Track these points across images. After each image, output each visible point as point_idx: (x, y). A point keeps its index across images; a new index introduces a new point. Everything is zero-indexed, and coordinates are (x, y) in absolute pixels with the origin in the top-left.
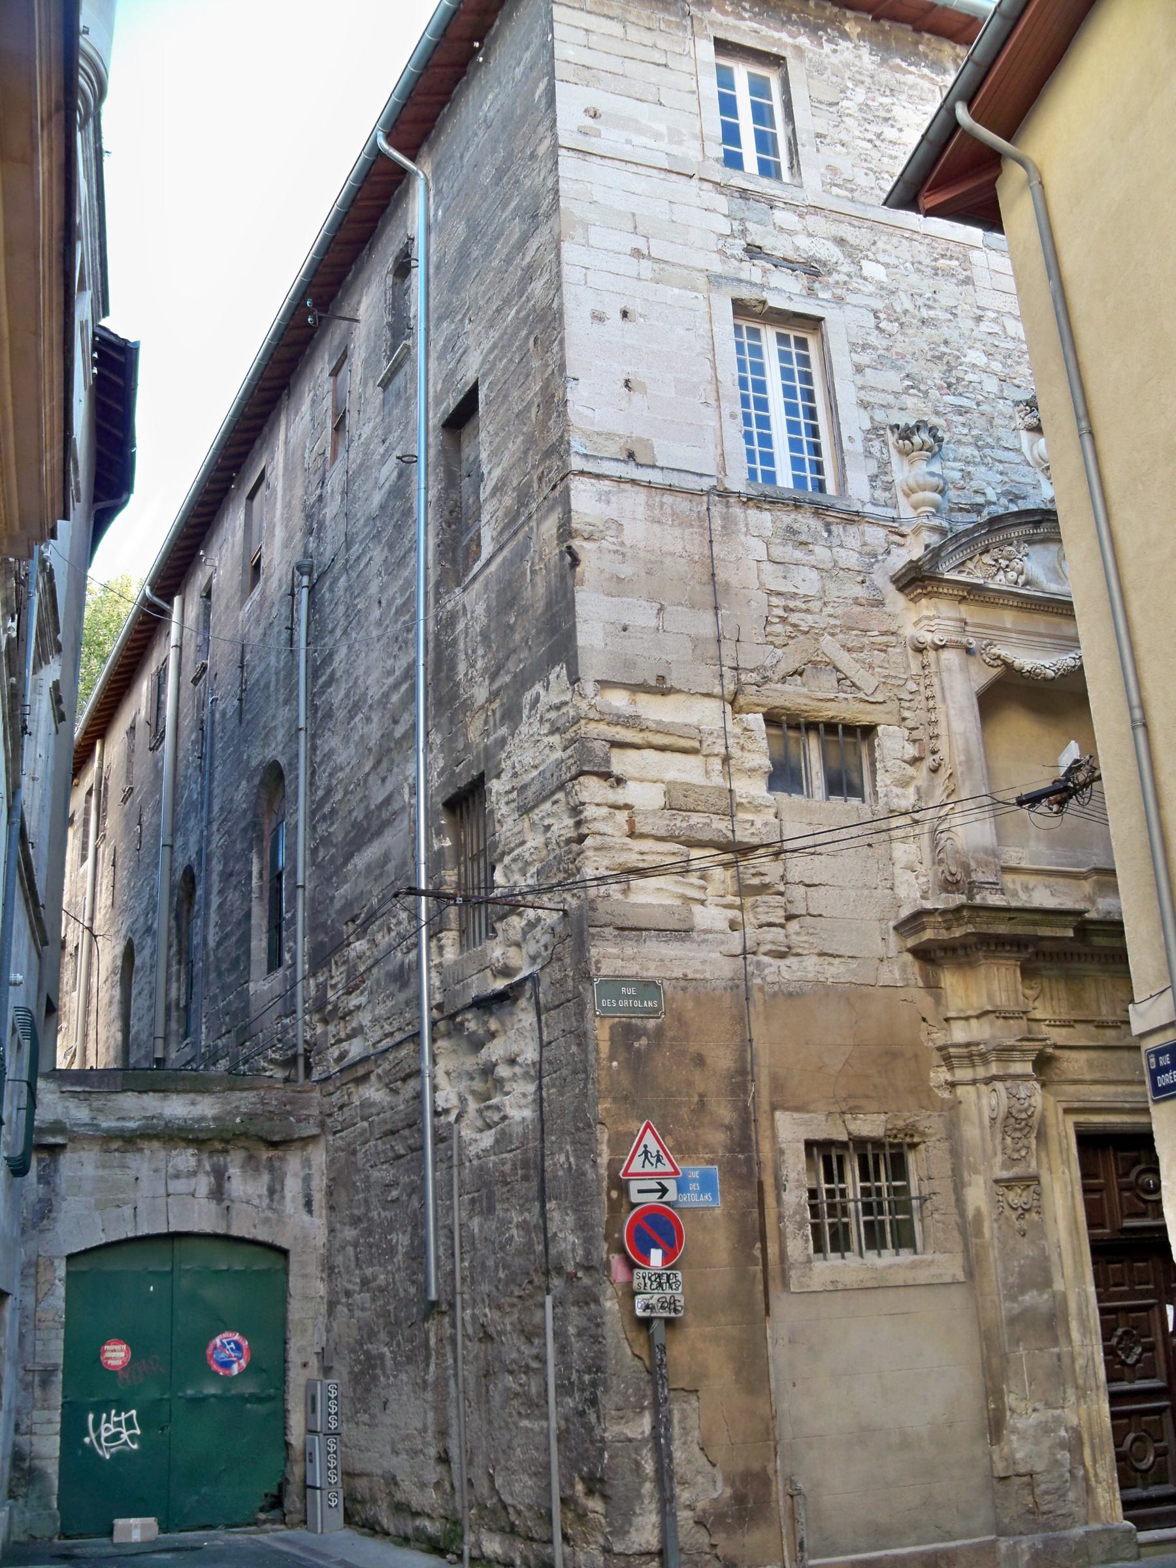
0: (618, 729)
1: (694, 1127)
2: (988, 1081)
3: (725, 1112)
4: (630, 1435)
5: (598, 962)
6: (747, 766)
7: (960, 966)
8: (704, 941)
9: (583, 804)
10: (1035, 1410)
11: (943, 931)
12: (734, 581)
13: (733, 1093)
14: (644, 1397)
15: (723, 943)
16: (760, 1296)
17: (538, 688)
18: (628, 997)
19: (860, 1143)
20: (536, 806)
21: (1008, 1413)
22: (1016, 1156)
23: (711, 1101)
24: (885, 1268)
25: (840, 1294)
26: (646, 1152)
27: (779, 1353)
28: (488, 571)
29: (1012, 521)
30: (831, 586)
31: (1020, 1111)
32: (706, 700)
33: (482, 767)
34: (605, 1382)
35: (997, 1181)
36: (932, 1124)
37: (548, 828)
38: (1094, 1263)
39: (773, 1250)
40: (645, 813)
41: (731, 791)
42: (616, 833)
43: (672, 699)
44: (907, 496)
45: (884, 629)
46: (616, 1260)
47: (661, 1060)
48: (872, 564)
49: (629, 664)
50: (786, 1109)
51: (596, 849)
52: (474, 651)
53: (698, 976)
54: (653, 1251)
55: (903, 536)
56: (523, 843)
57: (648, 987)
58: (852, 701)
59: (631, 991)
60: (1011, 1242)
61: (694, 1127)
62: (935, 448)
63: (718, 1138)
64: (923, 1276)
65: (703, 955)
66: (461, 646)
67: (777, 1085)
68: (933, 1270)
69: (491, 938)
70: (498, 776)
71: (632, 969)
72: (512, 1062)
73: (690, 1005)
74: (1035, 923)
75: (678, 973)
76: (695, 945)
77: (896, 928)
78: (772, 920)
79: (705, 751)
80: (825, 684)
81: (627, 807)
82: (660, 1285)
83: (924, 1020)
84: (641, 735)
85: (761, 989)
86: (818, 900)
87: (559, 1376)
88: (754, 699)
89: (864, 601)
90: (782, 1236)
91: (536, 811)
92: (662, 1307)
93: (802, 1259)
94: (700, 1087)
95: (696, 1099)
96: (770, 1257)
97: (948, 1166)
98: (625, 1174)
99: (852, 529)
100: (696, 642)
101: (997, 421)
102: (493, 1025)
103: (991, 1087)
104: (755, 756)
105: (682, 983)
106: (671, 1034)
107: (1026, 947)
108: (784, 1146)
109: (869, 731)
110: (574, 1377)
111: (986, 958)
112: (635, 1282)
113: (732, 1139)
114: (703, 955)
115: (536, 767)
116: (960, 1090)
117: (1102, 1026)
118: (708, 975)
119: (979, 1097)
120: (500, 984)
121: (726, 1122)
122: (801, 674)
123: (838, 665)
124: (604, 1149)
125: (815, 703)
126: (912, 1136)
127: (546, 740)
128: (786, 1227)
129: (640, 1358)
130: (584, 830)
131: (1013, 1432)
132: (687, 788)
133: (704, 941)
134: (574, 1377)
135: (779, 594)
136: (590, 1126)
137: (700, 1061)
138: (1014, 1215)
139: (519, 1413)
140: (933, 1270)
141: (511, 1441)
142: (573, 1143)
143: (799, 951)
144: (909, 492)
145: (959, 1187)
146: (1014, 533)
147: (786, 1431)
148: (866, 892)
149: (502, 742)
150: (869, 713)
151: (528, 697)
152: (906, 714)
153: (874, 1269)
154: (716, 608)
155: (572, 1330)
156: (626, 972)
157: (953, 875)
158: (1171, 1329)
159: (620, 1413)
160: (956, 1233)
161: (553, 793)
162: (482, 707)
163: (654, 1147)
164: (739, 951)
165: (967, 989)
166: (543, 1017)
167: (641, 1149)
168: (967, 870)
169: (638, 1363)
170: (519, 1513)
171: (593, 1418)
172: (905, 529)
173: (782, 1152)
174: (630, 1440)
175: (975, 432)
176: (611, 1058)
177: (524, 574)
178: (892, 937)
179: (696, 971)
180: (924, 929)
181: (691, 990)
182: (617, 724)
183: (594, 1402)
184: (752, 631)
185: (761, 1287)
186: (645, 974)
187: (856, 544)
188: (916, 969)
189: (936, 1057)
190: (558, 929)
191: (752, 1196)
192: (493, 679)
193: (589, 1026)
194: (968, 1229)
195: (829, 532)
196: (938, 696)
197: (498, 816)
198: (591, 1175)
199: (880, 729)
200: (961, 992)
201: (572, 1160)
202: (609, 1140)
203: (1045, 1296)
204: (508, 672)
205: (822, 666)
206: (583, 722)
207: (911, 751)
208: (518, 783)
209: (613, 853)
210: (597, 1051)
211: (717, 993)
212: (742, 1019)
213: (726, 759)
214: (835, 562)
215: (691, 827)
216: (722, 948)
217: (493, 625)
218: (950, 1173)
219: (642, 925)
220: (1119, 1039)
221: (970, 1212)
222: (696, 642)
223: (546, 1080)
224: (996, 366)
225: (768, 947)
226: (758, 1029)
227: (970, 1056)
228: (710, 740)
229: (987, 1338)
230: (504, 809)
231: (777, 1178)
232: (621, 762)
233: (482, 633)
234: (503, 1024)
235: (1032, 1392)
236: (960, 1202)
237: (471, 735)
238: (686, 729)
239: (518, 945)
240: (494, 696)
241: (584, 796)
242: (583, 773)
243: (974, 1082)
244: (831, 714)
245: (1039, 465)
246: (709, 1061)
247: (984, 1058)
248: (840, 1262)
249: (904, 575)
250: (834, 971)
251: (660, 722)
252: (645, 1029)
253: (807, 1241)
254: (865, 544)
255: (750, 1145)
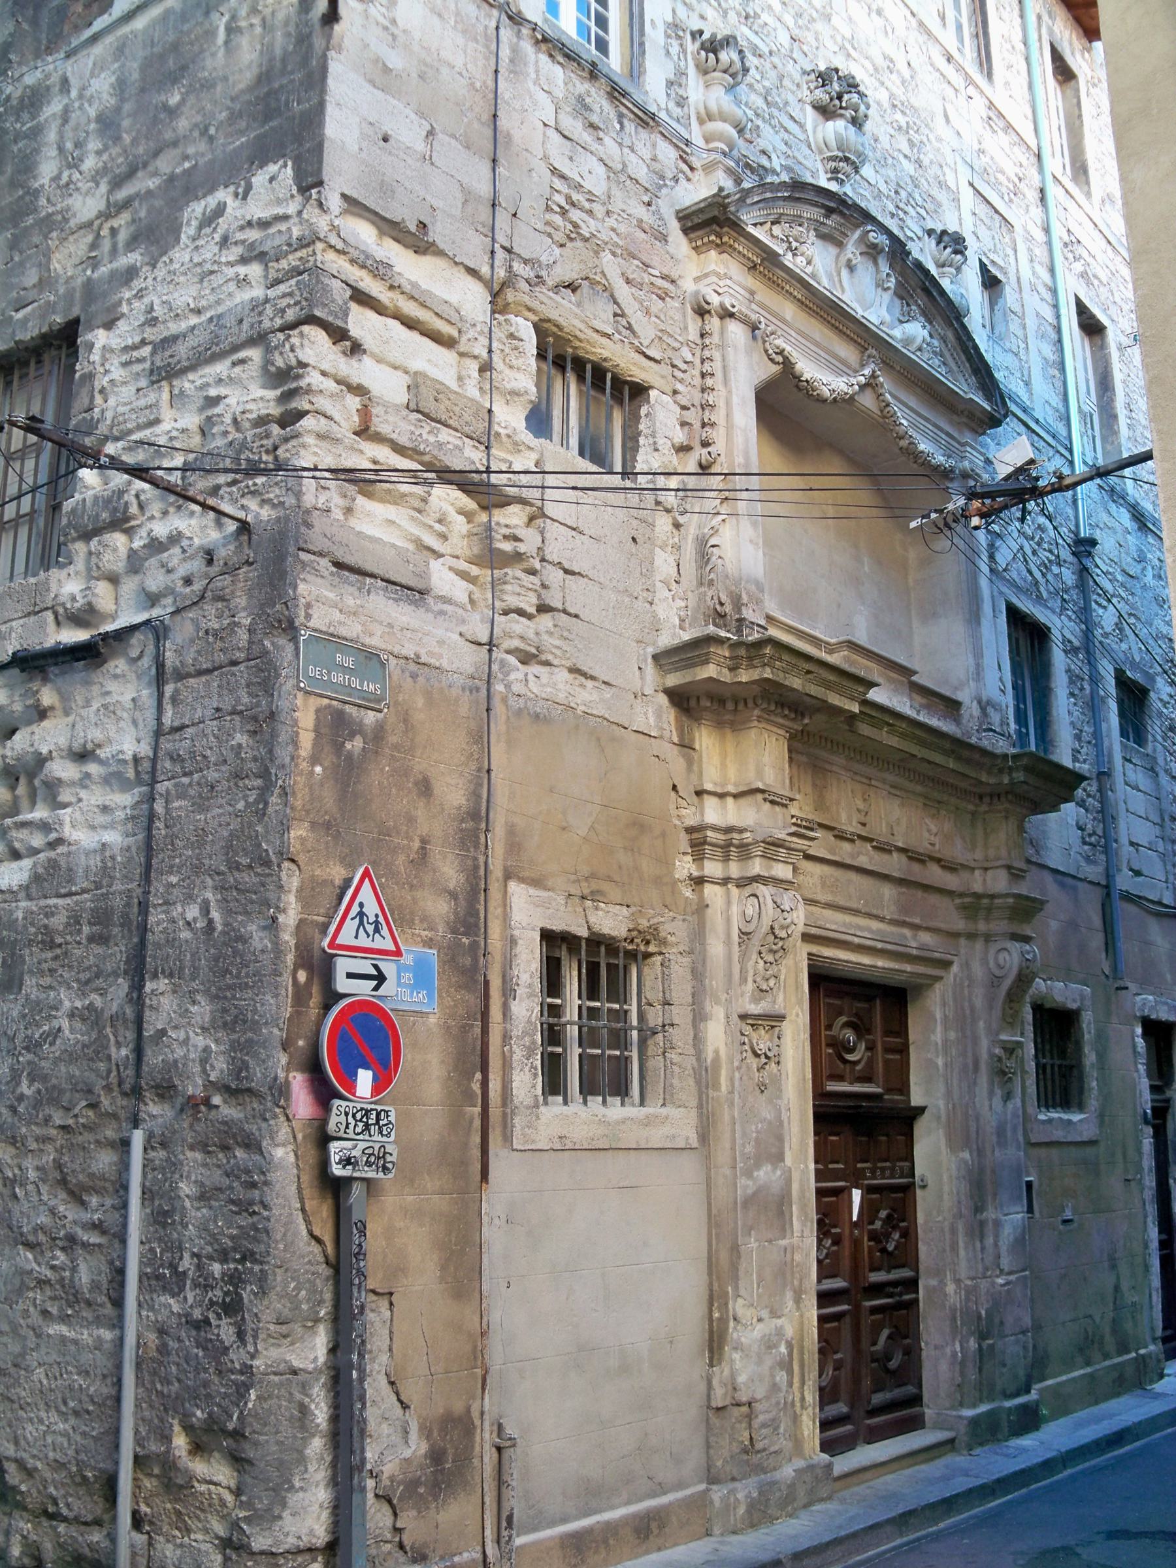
0: (363, 273)
1: (412, 887)
2: (744, 882)
3: (450, 872)
4: (296, 1363)
5: (308, 606)
6: (508, 386)
7: (719, 725)
8: (442, 613)
9: (303, 365)
10: (760, 1320)
11: (725, 671)
12: (517, 135)
13: (463, 845)
14: (321, 1302)
15: (463, 621)
16: (476, 1153)
17: (223, 195)
18: (345, 669)
19: (596, 941)
20: (193, 368)
21: (732, 1324)
22: (765, 987)
23: (435, 850)
24: (618, 1123)
25: (567, 1154)
26: (361, 914)
27: (494, 1234)
28: (126, 29)
29: (810, 196)
30: (617, 194)
31: (782, 927)
32: (469, 278)
33: (76, 311)
34: (262, 1279)
35: (743, 1017)
36: (676, 930)
37: (215, 401)
38: (816, 1133)
39: (495, 1085)
40: (386, 406)
41: (490, 411)
42: (343, 423)
43: (428, 261)
44: (701, 122)
45: (665, 271)
46: (298, 1083)
47: (378, 775)
48: (660, 187)
49: (386, 189)
50: (522, 880)
51: (321, 436)
52: (78, 145)
53: (432, 661)
54: (361, 1071)
55: (692, 169)
56: (157, 421)
57: (371, 659)
58: (627, 346)
59: (348, 662)
60: (751, 1099)
61: (412, 887)
62: (736, 75)
63: (440, 908)
64: (656, 1137)
65: (440, 632)
66: (52, 136)
67: (514, 846)
68: (667, 1130)
69: (61, 566)
70: (109, 325)
71: (352, 629)
72: (83, 755)
73: (420, 702)
74: (828, 686)
75: (409, 650)
76: (430, 615)
77: (655, 657)
78: (523, 605)
79: (462, 347)
80: (601, 315)
81: (359, 390)
82: (367, 1126)
83: (674, 788)
84: (390, 294)
85: (504, 700)
86: (576, 595)
87: (148, 1258)
88: (526, 299)
89: (647, 228)
90: (507, 1066)
91: (191, 376)
92: (368, 1164)
93: (529, 1101)
94: (423, 828)
95: (416, 844)
96: (492, 1094)
97: (689, 990)
98: (332, 945)
99: (644, 134)
100: (468, 196)
101: (786, 82)
102: (48, 697)
103: (748, 890)
104: (519, 376)
105: (412, 667)
106: (393, 739)
107: (803, 715)
108: (516, 933)
109: (639, 391)
110: (187, 1263)
111: (760, 719)
112: (333, 1120)
113: (456, 913)
114: (440, 632)
115: (198, 312)
116: (708, 889)
117: (841, 836)
118: (445, 664)
119: (729, 903)
120: (80, 636)
121: (451, 886)
122: (574, 291)
123: (617, 295)
124: (291, 900)
125: (590, 332)
126: (648, 943)
127: (230, 272)
128: (511, 1051)
129: (318, 1240)
130: (302, 403)
131: (736, 1349)
132: (440, 390)
133: (442, 613)
134: (187, 1263)
135: (563, 177)
136: (267, 863)
137: (425, 788)
138: (754, 1063)
139: (45, 1313)
140: (667, 1130)
141: (22, 1355)
142: (221, 888)
143: (550, 657)
144: (707, 117)
145: (699, 1017)
146: (810, 212)
147: (496, 1355)
148: (627, 600)
149: (131, 273)
150: (643, 368)
151: (197, 209)
152: (679, 387)
153: (603, 1122)
154: (494, 161)
155: (186, 1188)
156: (343, 631)
157: (722, 604)
158: (855, 1218)
159: (284, 1329)
160: (691, 1081)
161: (235, 348)
162: (89, 225)
163: (372, 909)
164: (485, 639)
165: (724, 755)
166: (169, 689)
167: (355, 909)
168: (738, 605)
169: (316, 1249)
170: (29, 1473)
171: (226, 1331)
172: (697, 163)
173: (513, 942)
174: (295, 1372)
175: (767, 84)
176: (314, 760)
177: (211, 33)
178: (650, 668)
179: (430, 653)
180: (707, 662)
181: (421, 679)
182: (363, 267)
183: (232, 1307)
184: (531, 210)
185: (478, 1140)
186: (367, 641)
187: (646, 154)
188: (672, 718)
189: (683, 842)
190: (222, 553)
191: (473, 1000)
192: (117, 183)
193: (283, 704)
194: (705, 1077)
195: (621, 123)
196: (719, 375)
197: (101, 381)
198: (259, 939)
199: (653, 393)
200: (716, 760)
201: (215, 915)
202: (300, 890)
203: (779, 1173)
204: (155, 174)
205: (600, 288)
206: (319, 246)
207: (680, 436)
208: (151, 334)
209: (340, 449)
210: (295, 742)
211: (455, 692)
212: (481, 738)
213: (486, 367)
214: (624, 165)
215: (440, 445)
216: (463, 629)
217: (127, 107)
218: (690, 1000)
219: (369, 567)
220: (853, 856)
221: (710, 1055)
222: (468, 196)
223: (160, 788)
224: (789, 20)
225: (516, 643)
226: (498, 755)
227: (729, 844)
228: (472, 334)
229: (713, 1222)
230: (117, 373)
231: (506, 979)
232: (361, 323)
233: (100, 119)
234: (65, 698)
235: (759, 1296)
236: (698, 1041)
237: (55, 265)
238: (445, 307)
239: (114, 579)
240: (112, 210)
241: (306, 355)
242: (311, 320)
243: (725, 881)
244: (606, 354)
245: (821, 152)
246: (437, 791)
247: (745, 852)
248: (602, 1110)
249: (701, 211)
250: (586, 696)
251: (415, 285)
252: (361, 724)
253: (535, 1075)
254: (654, 159)
255: (477, 925)
